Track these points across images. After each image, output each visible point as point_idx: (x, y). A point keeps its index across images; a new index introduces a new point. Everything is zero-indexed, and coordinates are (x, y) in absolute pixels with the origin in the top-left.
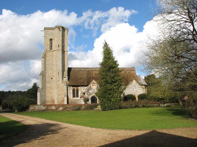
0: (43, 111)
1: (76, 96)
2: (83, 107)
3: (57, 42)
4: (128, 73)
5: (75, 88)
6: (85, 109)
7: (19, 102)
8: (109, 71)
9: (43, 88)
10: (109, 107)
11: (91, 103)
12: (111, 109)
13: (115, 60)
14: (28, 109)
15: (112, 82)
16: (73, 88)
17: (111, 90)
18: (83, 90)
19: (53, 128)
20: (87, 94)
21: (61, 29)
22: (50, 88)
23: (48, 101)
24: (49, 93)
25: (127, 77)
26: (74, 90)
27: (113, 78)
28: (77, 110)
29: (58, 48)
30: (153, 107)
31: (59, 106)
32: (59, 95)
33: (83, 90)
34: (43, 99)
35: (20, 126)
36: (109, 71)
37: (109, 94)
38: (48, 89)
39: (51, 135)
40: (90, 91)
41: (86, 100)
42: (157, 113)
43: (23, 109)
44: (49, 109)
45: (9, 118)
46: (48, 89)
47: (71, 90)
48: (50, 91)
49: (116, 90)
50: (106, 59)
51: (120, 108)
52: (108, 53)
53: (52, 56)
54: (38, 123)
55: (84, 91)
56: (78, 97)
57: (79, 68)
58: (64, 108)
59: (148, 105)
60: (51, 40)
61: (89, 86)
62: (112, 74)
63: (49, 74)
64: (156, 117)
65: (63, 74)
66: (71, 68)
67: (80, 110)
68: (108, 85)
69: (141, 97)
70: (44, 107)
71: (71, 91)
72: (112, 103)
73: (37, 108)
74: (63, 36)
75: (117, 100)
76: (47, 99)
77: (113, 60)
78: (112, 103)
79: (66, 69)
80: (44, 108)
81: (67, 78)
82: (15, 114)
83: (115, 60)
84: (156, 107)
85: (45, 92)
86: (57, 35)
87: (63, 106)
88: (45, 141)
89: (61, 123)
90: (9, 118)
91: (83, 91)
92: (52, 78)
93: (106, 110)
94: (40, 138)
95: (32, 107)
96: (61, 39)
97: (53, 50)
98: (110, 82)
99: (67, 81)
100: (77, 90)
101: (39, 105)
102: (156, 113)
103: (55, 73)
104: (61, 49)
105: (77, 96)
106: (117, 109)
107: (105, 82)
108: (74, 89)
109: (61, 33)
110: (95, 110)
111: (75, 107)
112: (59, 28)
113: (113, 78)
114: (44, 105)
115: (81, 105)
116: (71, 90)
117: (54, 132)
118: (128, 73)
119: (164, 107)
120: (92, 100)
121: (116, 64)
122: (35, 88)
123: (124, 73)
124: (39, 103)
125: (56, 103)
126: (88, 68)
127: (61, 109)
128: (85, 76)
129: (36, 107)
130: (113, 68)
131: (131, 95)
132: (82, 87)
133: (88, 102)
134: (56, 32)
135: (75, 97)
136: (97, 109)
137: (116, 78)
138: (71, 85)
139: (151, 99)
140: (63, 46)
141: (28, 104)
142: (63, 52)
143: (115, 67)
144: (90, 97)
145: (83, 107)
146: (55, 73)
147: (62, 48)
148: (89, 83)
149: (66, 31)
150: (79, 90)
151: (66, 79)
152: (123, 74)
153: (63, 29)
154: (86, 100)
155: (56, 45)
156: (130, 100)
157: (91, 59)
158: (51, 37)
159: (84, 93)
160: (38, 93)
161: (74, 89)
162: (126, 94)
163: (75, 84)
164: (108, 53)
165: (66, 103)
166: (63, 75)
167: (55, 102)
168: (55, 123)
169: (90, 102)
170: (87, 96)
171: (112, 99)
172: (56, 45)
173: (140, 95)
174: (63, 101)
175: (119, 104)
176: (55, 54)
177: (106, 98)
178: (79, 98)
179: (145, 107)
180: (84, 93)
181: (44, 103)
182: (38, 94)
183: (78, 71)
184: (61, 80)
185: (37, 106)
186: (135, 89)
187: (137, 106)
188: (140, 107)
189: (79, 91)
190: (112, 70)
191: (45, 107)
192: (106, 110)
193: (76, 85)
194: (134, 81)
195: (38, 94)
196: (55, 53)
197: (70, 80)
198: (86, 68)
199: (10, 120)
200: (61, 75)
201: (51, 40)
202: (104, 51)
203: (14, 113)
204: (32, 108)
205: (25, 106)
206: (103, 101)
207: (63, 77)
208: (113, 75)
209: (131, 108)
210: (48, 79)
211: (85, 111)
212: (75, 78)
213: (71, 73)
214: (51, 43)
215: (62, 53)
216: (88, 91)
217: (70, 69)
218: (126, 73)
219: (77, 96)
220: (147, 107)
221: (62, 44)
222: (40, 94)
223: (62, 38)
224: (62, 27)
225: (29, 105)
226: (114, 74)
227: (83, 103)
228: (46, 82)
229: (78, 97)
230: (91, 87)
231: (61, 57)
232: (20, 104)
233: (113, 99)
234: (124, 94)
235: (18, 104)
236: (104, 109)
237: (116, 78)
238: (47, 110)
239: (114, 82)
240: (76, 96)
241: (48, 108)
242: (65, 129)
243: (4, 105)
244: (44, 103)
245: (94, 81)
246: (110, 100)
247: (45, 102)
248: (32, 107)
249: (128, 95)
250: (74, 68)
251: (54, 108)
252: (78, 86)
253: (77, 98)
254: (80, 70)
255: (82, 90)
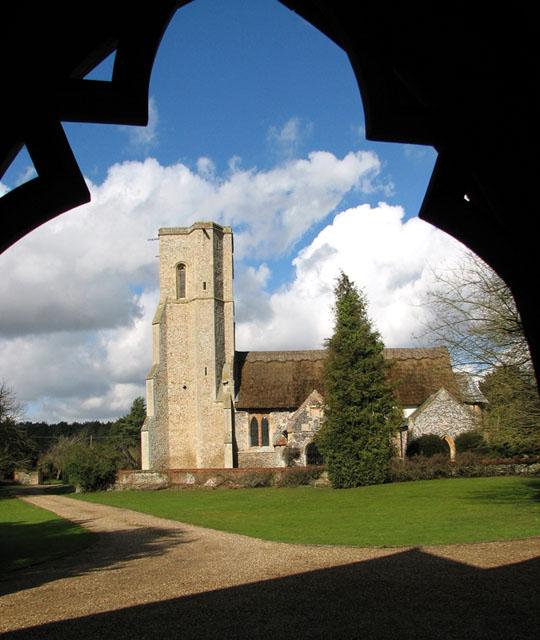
0: (159, 489)
1: (260, 440)
2: (278, 477)
3: (199, 272)
4: (425, 366)
5: (259, 417)
6: (282, 485)
7: (85, 462)
8: (353, 363)
9: (157, 419)
10: (353, 478)
11: (308, 462)
12: (359, 485)
13: (373, 330)
14: (113, 483)
15: (363, 399)
16: (252, 416)
17: (359, 423)
18: (284, 422)
19: (160, 541)
20: (296, 437)
21: (210, 232)
22: (179, 416)
23: (176, 459)
24: (455, 304)
25: (419, 379)
26: (253, 423)
27: (367, 387)
28: (258, 485)
29: (201, 293)
30: (493, 474)
31: (206, 473)
32: (206, 439)
33: (284, 422)
34: (158, 453)
35: (76, 535)
36: (353, 363)
37: (355, 438)
38: (175, 420)
39: (148, 559)
40: (305, 427)
41: (292, 455)
42: (490, 496)
43: (98, 482)
44: (175, 484)
45: (54, 511)
46: (175, 420)
47: (244, 421)
48: (181, 426)
49: (377, 424)
50: (345, 329)
51: (388, 481)
52: (350, 306)
53: (185, 318)
54: (130, 528)
55: (284, 426)
56: (268, 444)
57: (270, 353)
58: (221, 479)
59: (477, 468)
60: (181, 266)
61: (301, 410)
62: (361, 375)
63: (176, 371)
64: (477, 509)
65: (221, 372)
66: (245, 354)
67: (269, 486)
68: (352, 408)
69: (465, 442)
70: (160, 476)
71: (246, 426)
72: (362, 463)
73: (140, 481)
74: (218, 253)
75: (377, 454)
76: (172, 453)
77: (368, 327)
78: (362, 463)
79: (230, 357)
80: (159, 481)
81: (231, 386)
82: (73, 498)
83: (373, 330)
84: (503, 474)
85: (165, 429)
86: (198, 252)
87: (217, 473)
88: (122, 573)
89: (191, 528)
90: (53, 513)
91: (283, 425)
92: (185, 387)
93: (345, 485)
94: (113, 566)
95: (124, 476)
96: (212, 263)
97: (187, 297)
98: (358, 400)
99: (233, 396)
100: (265, 423)
101: (145, 472)
102: (489, 497)
103: (193, 370)
104: (213, 296)
105: (266, 442)
106: (377, 482)
107: (341, 401)
108: (254, 419)
109: (210, 244)
110: (313, 486)
111: (253, 476)
112: (204, 230)
113: (367, 387)
114: (161, 473)
115: (270, 473)
116: (244, 421)
117: (157, 551)
118: (425, 366)
119: (526, 475)
120: (308, 456)
121: (374, 343)
122: (139, 409)
123: (414, 366)
124: (145, 466)
125: (199, 465)
126: (298, 353)
127: (211, 482)
128: (289, 378)
129: (138, 479)
130: (365, 356)
131: (432, 435)
132: (279, 414)
133: (297, 462)
134: (196, 241)
135: (257, 445)
136: (320, 482)
137: (374, 387)
138: (246, 406)
139: (485, 451)
140: (218, 286)
141: (113, 468)
142: (219, 303)
143: (371, 352)
144: (303, 445)
145: (278, 477)
146: (194, 371)
147: (215, 292)
148: (301, 399)
149: (227, 239)
150: (270, 421)
151: (228, 389)
152: (408, 370)
153: (218, 231)
154: (290, 454)
155: (196, 282)
156: (419, 454)
157: (302, 320)
158: (180, 259)
159: (286, 433)
160: (143, 433)
161: (254, 419)
162: (417, 434)
163: (256, 405)
164: (350, 306)
165: (229, 464)
166: (219, 376)
167: (195, 461)
168: (170, 527)
169: (303, 461)
170: (294, 441)
171: (364, 452)
172: (196, 282)
173: (463, 436)
174: (221, 457)
175: (385, 467)
176: (192, 312)
177: (346, 448)
178: (270, 448)
179: (467, 476)
180: (286, 433)
181: (161, 468)
182: (145, 436)
183: (268, 362)
184: (214, 392)
185: (140, 475)
186: (439, 419)
187: (440, 472)
188: (452, 476)
189: (271, 426)
190: (361, 362)
191: (165, 477)
192: (345, 485)
193: (261, 406)
194: (443, 394)
195: (142, 437)
196: (192, 309)
197: (241, 391)
198: (293, 353)
199: (54, 518)
200: (214, 378)
201: (181, 266)
202: (340, 304)
203: (70, 497)
204: (123, 480)
205: (104, 473)
206: (334, 458)
207: (218, 383)
208: (365, 378)
209: (421, 478)
210: (173, 390)
211: (281, 490)
212: (257, 385)
213: (245, 369)
214: (181, 278)
215: (216, 308)
216: (297, 425)
217: (240, 357)
218: (420, 364)
219: (266, 442)
220: (472, 476)
221: (215, 279)
222: (151, 435)
223: (215, 261)
224: (214, 225)
225: (115, 472)
226: (368, 374)
227: (282, 464)
228: (167, 400)
229: (268, 444)
230: (305, 413)
231: (212, 319)
232: (90, 470)
233: (364, 454)
234: (410, 434)
235: (83, 468)
236: (339, 483)
237: (374, 387)
238: (170, 487)
239: (370, 400)
240: (260, 440)
241: (174, 481)
242: (192, 545)
243: (46, 471)
244: (161, 468)
245: (315, 395)
246: (357, 455)
247: (166, 460)
248: (124, 476)
249: (425, 436)
250: (256, 353)
251: (190, 480)
252: (272, 410)
253: (265, 449)
254: (274, 357)
255: (278, 421)
